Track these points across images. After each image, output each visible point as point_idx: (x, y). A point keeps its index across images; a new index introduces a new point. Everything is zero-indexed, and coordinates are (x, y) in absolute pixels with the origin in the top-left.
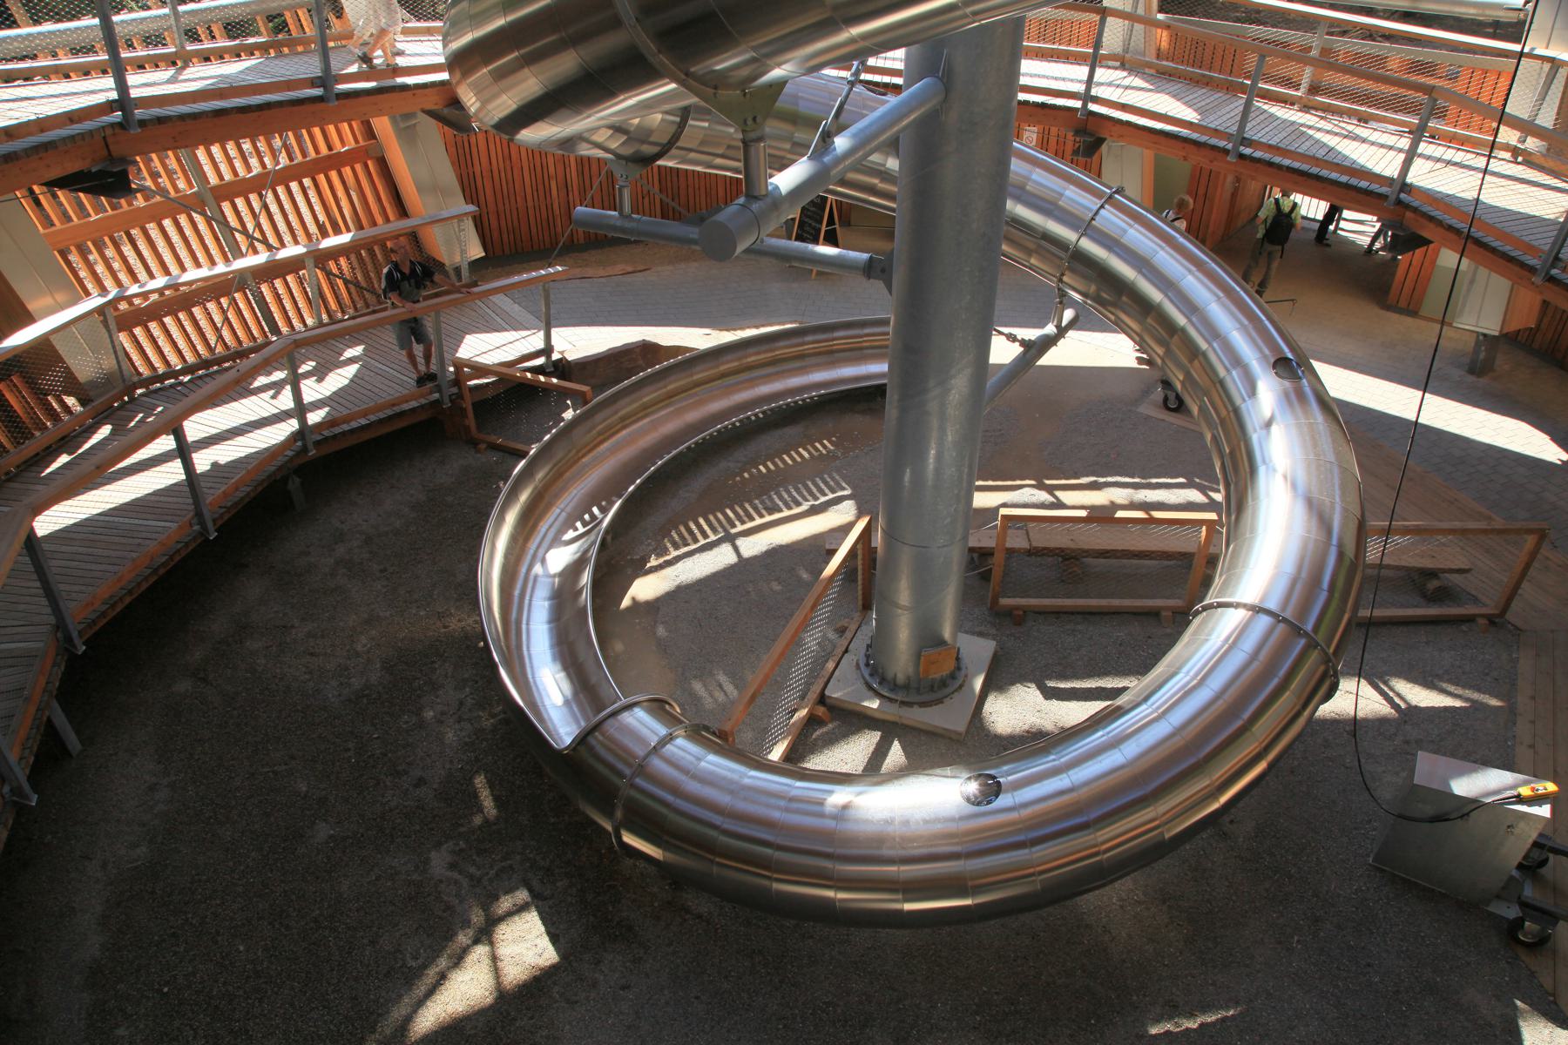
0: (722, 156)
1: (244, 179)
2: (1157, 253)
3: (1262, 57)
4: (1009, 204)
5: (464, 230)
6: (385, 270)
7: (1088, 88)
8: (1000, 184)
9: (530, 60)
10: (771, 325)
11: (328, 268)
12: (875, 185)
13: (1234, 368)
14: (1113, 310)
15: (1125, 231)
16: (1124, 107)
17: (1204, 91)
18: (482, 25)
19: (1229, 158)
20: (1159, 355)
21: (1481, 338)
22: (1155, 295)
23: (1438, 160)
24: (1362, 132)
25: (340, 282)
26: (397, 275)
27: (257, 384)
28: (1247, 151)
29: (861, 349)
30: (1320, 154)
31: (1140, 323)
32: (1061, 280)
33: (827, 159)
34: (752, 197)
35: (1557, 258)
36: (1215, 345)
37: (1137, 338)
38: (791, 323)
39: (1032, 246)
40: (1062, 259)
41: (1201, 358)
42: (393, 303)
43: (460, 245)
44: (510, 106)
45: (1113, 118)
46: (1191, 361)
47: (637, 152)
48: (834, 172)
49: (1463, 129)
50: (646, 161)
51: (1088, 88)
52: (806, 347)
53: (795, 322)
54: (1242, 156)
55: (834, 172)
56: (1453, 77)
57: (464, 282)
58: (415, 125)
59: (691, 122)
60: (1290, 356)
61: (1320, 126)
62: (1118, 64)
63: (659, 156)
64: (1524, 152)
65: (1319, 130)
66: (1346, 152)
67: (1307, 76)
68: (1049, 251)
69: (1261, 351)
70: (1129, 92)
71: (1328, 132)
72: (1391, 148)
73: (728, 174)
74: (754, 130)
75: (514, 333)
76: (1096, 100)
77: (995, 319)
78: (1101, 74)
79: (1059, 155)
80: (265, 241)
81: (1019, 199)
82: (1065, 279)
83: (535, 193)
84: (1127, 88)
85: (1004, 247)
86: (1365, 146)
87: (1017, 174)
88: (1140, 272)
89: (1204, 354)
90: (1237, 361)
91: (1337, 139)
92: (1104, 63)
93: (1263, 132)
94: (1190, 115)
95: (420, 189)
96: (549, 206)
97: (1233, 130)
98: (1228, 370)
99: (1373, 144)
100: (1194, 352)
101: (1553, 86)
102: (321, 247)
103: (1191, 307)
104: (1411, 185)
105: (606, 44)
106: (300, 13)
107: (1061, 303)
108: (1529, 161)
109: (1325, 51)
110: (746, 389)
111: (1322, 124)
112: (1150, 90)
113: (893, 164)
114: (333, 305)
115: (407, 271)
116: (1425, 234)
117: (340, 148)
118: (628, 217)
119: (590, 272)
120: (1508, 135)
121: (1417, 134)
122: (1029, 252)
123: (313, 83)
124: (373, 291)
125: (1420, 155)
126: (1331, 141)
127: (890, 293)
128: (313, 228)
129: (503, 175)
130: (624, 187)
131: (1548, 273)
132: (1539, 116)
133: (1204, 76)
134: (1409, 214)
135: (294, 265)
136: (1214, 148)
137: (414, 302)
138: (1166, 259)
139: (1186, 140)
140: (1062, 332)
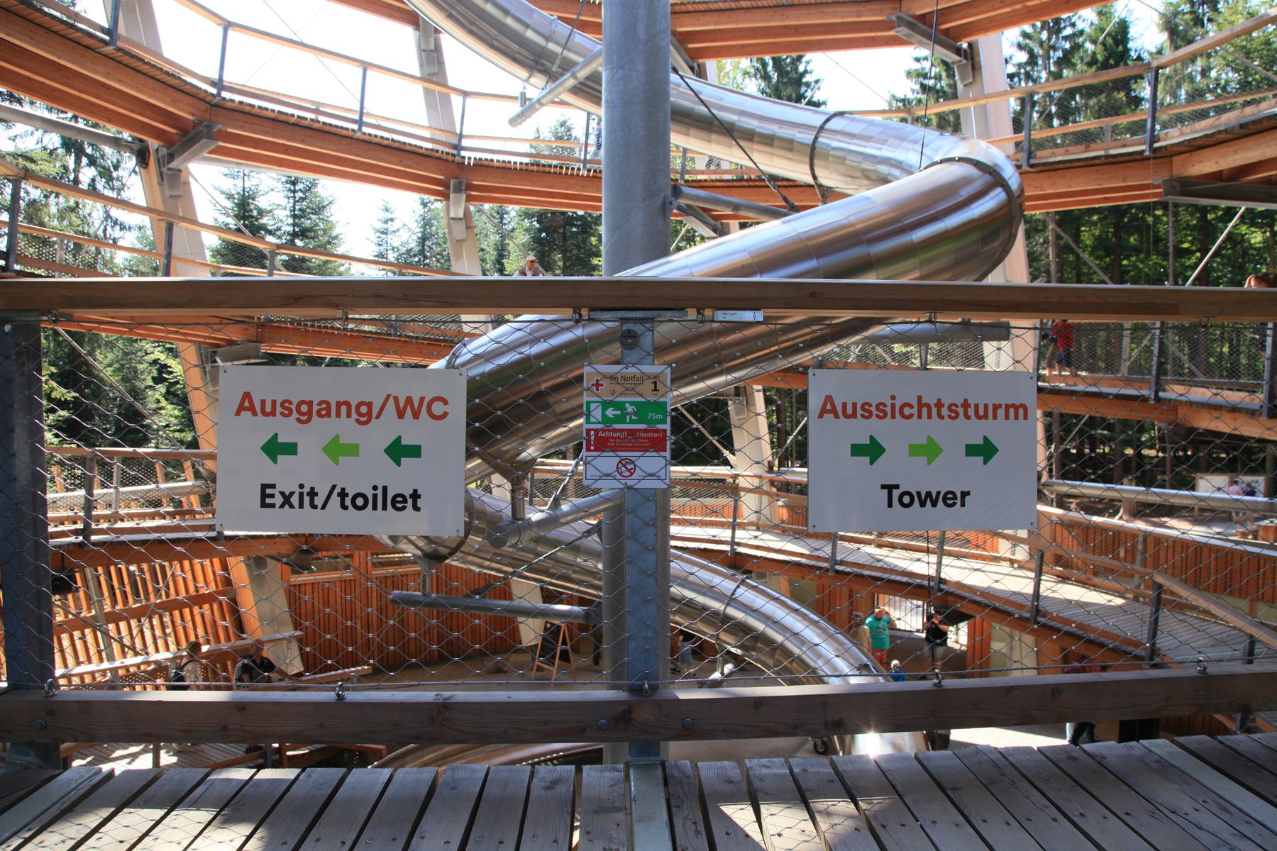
0: (489, 560)
15: (754, 601)
16: (757, 547)
18: (862, 8)
27: (115, 755)
54: (838, 572)
59: (471, 537)
76: (739, 544)
80: (133, 648)
110: (502, 755)
117: (202, 591)
138: (778, 613)
139: (798, 564)
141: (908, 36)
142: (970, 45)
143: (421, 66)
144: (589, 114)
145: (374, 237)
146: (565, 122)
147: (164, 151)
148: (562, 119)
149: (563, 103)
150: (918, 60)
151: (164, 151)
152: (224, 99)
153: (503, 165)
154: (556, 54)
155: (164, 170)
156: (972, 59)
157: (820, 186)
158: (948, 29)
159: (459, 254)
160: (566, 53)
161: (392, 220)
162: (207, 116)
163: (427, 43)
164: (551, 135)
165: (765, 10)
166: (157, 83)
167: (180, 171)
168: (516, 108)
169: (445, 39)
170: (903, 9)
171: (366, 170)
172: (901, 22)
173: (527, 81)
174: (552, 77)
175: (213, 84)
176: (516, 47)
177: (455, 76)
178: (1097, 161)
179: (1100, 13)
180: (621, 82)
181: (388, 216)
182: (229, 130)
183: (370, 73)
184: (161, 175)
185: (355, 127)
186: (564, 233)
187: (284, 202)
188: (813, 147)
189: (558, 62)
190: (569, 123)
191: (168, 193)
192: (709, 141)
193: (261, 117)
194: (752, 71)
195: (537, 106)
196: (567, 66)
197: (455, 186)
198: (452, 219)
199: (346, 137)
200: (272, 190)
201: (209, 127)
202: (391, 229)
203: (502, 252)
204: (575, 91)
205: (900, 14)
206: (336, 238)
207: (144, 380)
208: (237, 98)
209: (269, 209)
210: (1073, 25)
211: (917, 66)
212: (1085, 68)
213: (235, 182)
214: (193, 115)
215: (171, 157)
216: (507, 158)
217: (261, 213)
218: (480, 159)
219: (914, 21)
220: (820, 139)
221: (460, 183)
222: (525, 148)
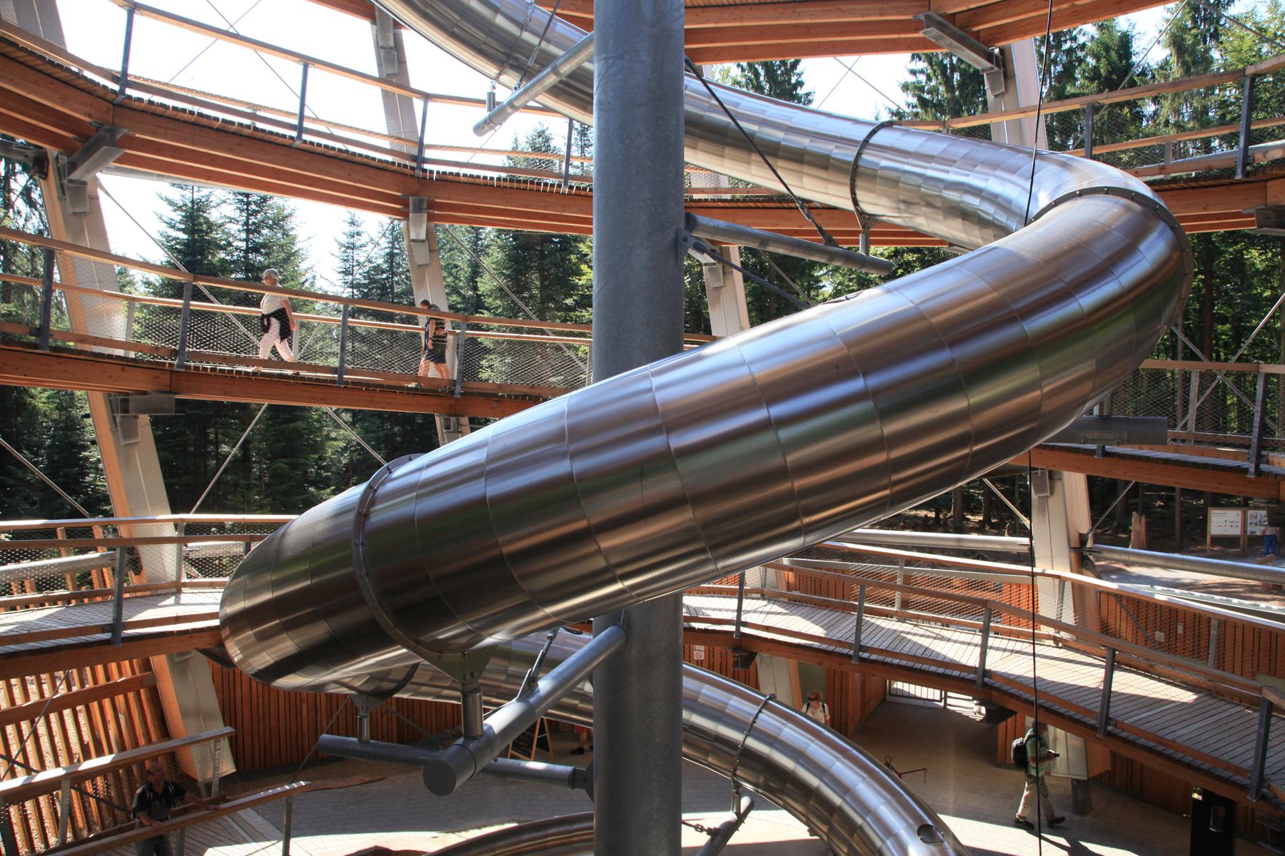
1: (21, 708)
2: (809, 745)
3: (863, 588)
4: (686, 715)
5: (219, 749)
6: (139, 791)
7: (739, 616)
8: (676, 699)
9: (287, 627)
10: (492, 825)
11: (83, 787)
12: (576, 705)
13: (888, 838)
14: (781, 796)
15: (781, 730)
16: (768, 629)
17: (826, 611)
19: (852, 662)
20: (824, 832)
21: (1075, 783)
22: (813, 781)
23: (1005, 650)
24: (946, 633)
25: (92, 801)
26: (150, 795)
28: (866, 655)
29: (573, 842)
30: (919, 653)
31: (805, 805)
32: (734, 774)
33: (532, 700)
34: (470, 737)
35: (1108, 719)
36: (868, 819)
37: (804, 819)
38: (510, 822)
39: (708, 747)
40: (734, 757)
41: (859, 831)
42: (141, 823)
43: (214, 762)
44: (268, 661)
45: (761, 637)
46: (851, 835)
47: (378, 688)
48: (539, 710)
49: (1016, 626)
50: (384, 695)
51: (739, 616)
52: (523, 845)
53: (513, 821)
54: (862, 660)
55: (539, 710)
56: (998, 589)
57: (213, 796)
58: (187, 660)
60: (930, 823)
61: (915, 632)
62: (759, 596)
63: (396, 690)
64: (1061, 640)
65: (915, 634)
66: (938, 650)
67: (898, 596)
68: (720, 749)
69: (906, 822)
70: (769, 616)
71: (922, 636)
72: (969, 644)
73: (454, 702)
74: (472, 683)
75: (254, 844)
76: (746, 624)
77: (683, 806)
78: (747, 604)
79: (723, 672)
80: (26, 765)
81: (693, 710)
82: (738, 773)
83: (288, 714)
84: (768, 613)
85: (684, 749)
86: (950, 644)
87: (689, 689)
88: (798, 762)
89: (861, 828)
90: (889, 832)
91: (929, 640)
92: (749, 595)
93: (874, 640)
94: (818, 631)
95: (185, 713)
96: (299, 726)
97: (852, 640)
98: (882, 840)
99: (955, 642)
100: (853, 828)
101: (1065, 594)
102: (81, 768)
103: (843, 789)
104: (990, 671)
105: (354, 617)
106: (104, 570)
107: (737, 793)
108: (1067, 646)
109: (907, 579)
111: (916, 630)
112: (785, 614)
113: (588, 687)
114: (80, 822)
115: (160, 791)
116: (1010, 707)
118: (367, 742)
119: (331, 783)
120: (1045, 630)
121: (985, 631)
122: (706, 753)
123: (103, 629)
124: (123, 808)
125: (991, 648)
126: (926, 642)
127: (592, 799)
128: (76, 748)
129: (261, 700)
130: (364, 717)
131: (1105, 729)
132: (1063, 615)
133: (825, 600)
134: (994, 693)
135: (49, 787)
136: (840, 654)
137: (162, 820)
139: (817, 650)
140: (741, 817)
141: (937, 38)
142: (1002, 51)
143: (380, 65)
144: (571, 120)
145: (338, 252)
146: (543, 132)
147: (64, 160)
148: (540, 129)
149: (545, 109)
150: (913, 72)
151: (64, 160)
152: (130, 97)
153: (471, 180)
154: (532, 46)
155: (65, 181)
156: (1004, 66)
157: (862, 213)
158: (979, 31)
159: (421, 283)
160: (544, 45)
161: (358, 234)
162: (110, 119)
163: (385, 38)
164: (528, 146)
165: (774, 7)
166: (40, 75)
167: (84, 183)
168: (482, 113)
169: (408, 37)
170: (932, 7)
171: (310, 185)
172: (930, 21)
173: (497, 79)
174: (526, 73)
175: (114, 78)
176: (482, 36)
177: (417, 79)
178: (1174, 186)
179: (1101, 27)
180: (619, 77)
181: (354, 229)
182: (137, 135)
183: (312, 71)
184: (62, 188)
185: (294, 134)
186: (541, 251)
187: (236, 214)
188: (855, 165)
189: (535, 55)
190: (547, 133)
191: (70, 210)
192: (722, 156)
193: (178, 120)
194: (744, 80)
195: (509, 110)
196: (546, 60)
197: (415, 205)
198: (413, 241)
199: (284, 145)
200: (225, 202)
201: (112, 132)
202: (358, 244)
203: (476, 270)
204: (555, 91)
205: (928, 13)
206: (294, 254)
207: (82, 407)
208: (146, 96)
209: (220, 222)
210: (1074, 39)
211: (912, 79)
212: (1087, 83)
213: (184, 192)
214: (90, 116)
215: (73, 166)
216: (475, 172)
217: (211, 226)
218: (444, 173)
219: (945, 22)
220: (864, 156)
221: (421, 201)
222: (501, 161)
